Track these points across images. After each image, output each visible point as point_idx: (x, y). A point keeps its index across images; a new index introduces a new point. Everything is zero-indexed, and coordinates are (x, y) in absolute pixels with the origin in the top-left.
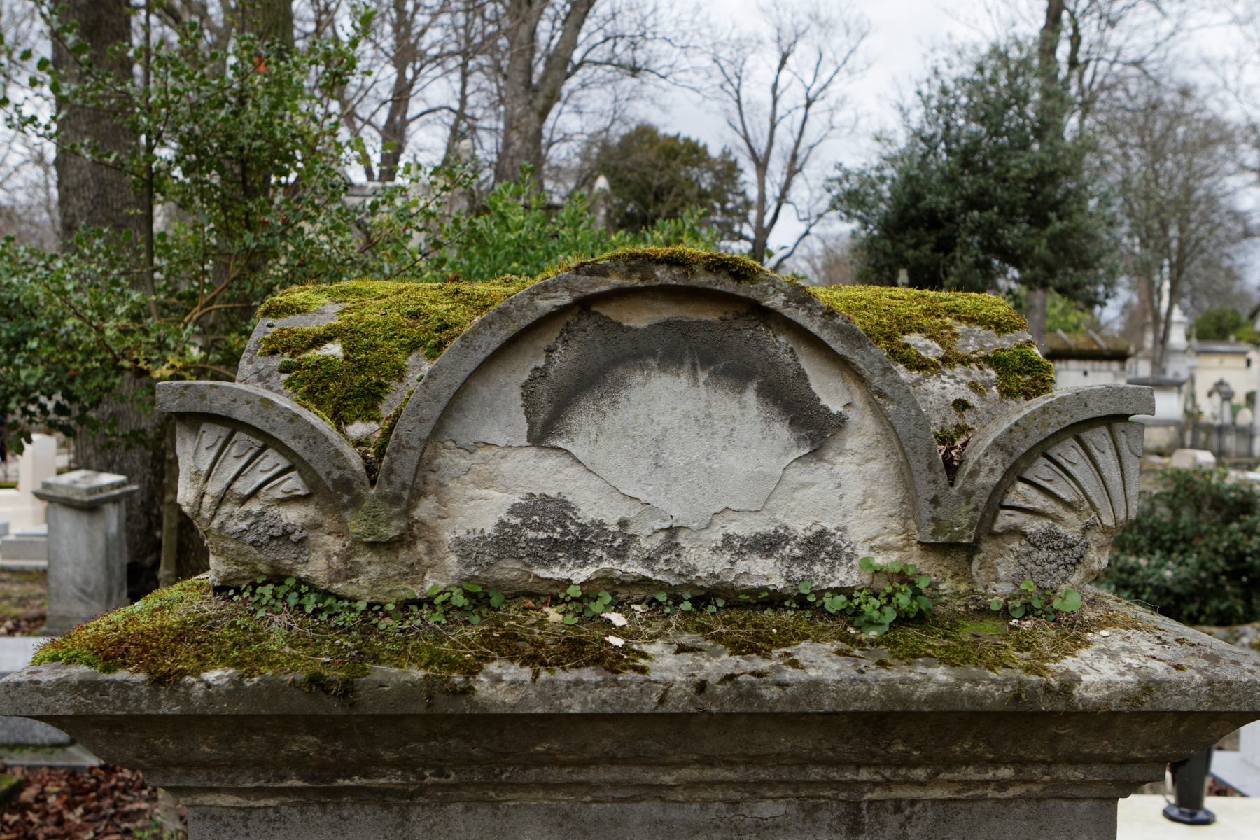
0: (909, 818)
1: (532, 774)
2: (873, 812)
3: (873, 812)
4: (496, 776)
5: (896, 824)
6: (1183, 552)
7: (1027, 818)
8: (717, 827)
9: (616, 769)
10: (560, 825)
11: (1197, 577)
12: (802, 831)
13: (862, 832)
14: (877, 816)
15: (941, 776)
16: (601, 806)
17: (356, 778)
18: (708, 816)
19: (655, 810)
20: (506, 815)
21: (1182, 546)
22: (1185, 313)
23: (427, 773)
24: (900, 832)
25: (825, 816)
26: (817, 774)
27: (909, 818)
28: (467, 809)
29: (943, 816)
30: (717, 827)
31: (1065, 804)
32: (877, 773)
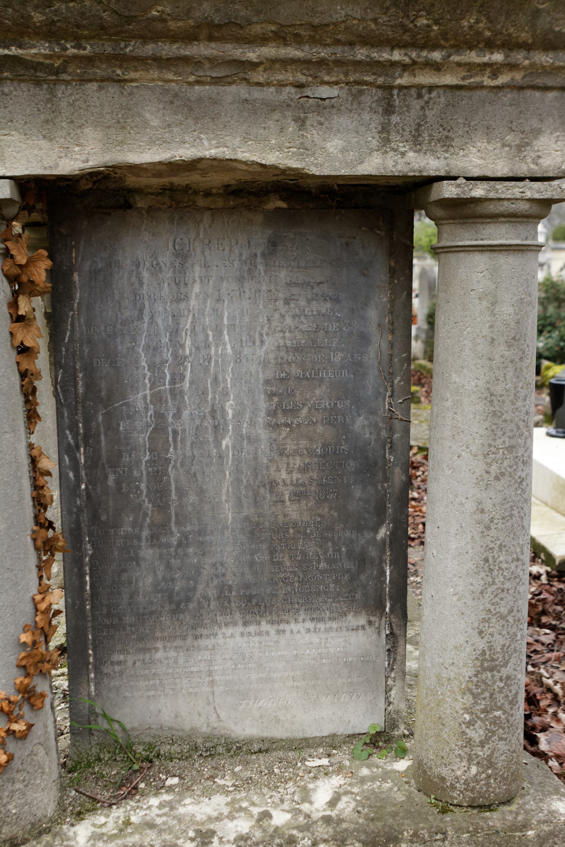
0: (427, 102)
1: (149, 49)
2: (402, 97)
3: (402, 97)
4: (121, 49)
5: (418, 107)
6: (549, 332)
7: (511, 105)
8: (289, 105)
9: (213, 45)
10: (172, 103)
11: (558, 345)
12: (350, 111)
13: (394, 113)
14: (405, 100)
15: (452, 58)
16: (202, 88)
17: (13, 48)
18: (281, 97)
19: (243, 92)
20: (131, 94)
21: (549, 328)
22: (545, 227)
23: (68, 46)
24: (421, 113)
25: (367, 99)
26: (362, 54)
27: (427, 102)
28: (100, 88)
29: (452, 102)
30: (289, 105)
31: (537, 94)
32: (406, 54)
